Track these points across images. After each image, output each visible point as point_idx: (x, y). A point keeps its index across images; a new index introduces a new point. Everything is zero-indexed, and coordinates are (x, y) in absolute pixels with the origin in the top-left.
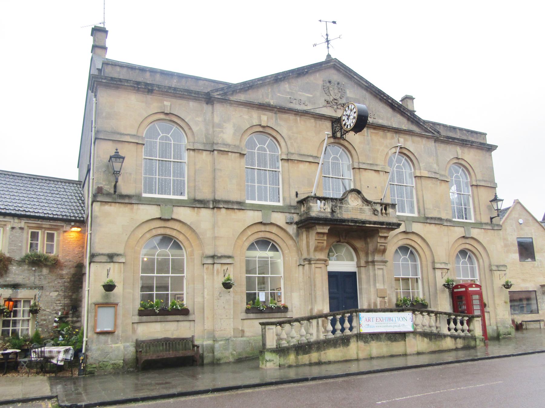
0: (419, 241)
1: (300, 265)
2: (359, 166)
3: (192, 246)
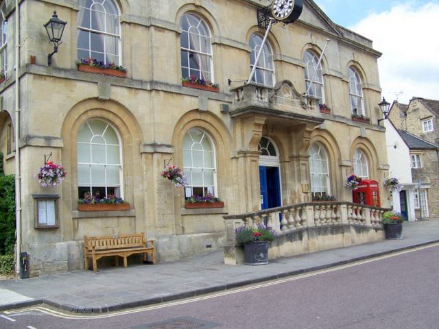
0: (329, 138)
1: (235, 158)
2: (220, 40)
3: (129, 132)
